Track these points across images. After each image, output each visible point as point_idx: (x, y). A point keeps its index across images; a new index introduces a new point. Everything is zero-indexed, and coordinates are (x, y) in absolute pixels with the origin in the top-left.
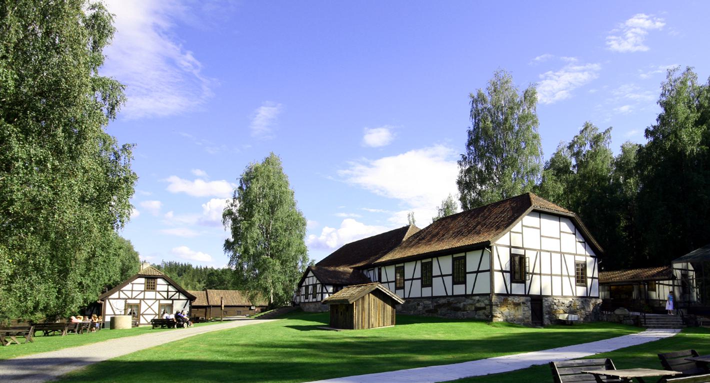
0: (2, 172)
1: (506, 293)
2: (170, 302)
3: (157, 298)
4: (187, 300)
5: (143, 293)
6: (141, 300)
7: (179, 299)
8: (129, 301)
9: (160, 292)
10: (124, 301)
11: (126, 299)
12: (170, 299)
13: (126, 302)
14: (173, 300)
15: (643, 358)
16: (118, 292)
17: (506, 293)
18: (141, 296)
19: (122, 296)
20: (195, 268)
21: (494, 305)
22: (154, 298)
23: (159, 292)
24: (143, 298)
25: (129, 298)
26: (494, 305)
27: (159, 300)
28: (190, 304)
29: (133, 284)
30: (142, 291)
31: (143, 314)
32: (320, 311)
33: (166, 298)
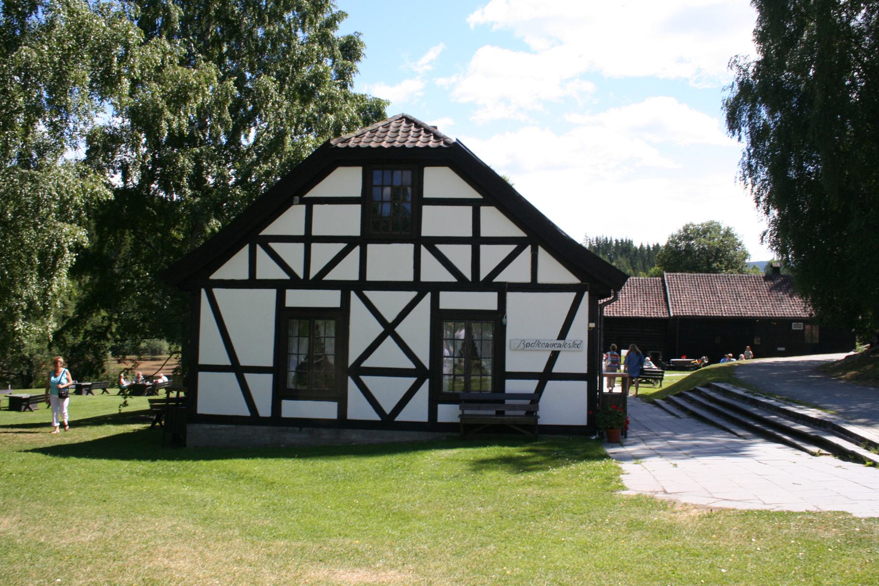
0: (196, 2)
1: (246, 412)
2: (487, 301)
3: (425, 277)
4: (578, 290)
5: (356, 251)
6: (345, 287)
7: (533, 286)
8: (296, 298)
9: (441, 248)
10: (272, 293)
11: (281, 287)
12: (488, 285)
13: (281, 299)
14: (503, 290)
15: (714, 385)
16: (245, 251)
17: (246, 412)
18: (347, 270)
19: (267, 269)
20: (638, 248)
21: (481, 385)
22: (408, 276)
23: (431, 243)
24: (355, 276)
25: (295, 283)
26: (481, 385)
27: (436, 288)
28: (594, 313)
29: (310, 203)
30: (350, 242)
31: (358, 371)
32: (49, 393)
33: (468, 274)
